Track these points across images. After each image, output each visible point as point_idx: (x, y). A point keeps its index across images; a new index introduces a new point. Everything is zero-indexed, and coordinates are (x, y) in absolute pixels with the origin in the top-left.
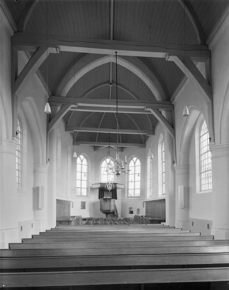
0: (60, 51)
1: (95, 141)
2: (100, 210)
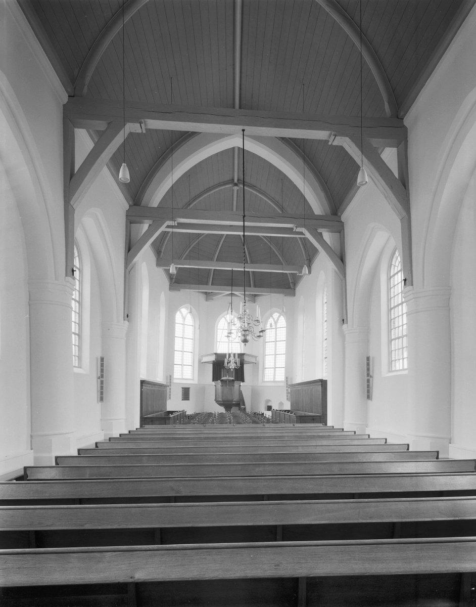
0: (146, 129)
1: (207, 284)
2: (216, 400)
